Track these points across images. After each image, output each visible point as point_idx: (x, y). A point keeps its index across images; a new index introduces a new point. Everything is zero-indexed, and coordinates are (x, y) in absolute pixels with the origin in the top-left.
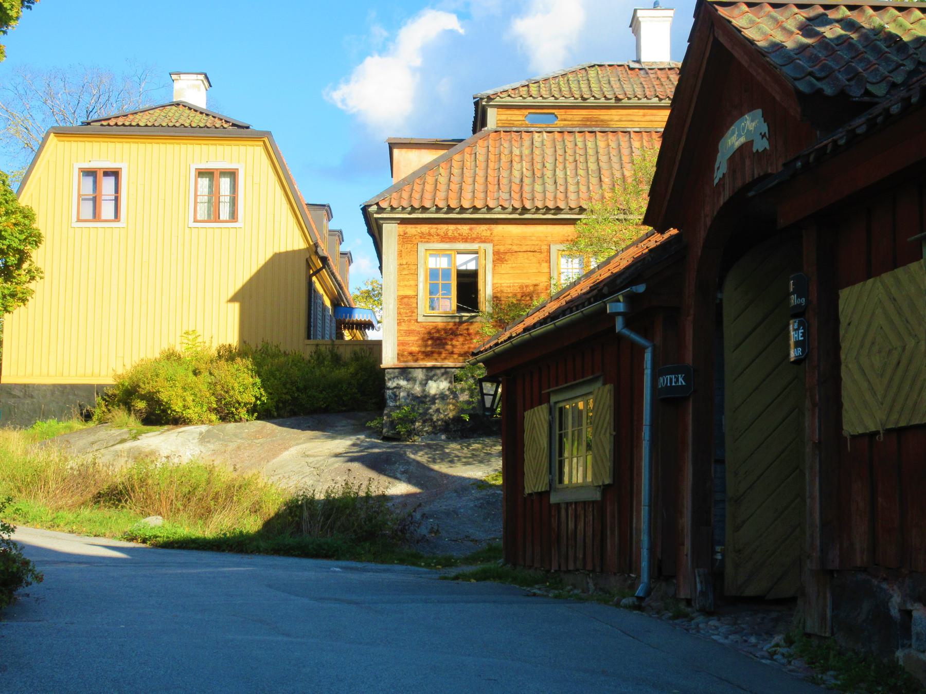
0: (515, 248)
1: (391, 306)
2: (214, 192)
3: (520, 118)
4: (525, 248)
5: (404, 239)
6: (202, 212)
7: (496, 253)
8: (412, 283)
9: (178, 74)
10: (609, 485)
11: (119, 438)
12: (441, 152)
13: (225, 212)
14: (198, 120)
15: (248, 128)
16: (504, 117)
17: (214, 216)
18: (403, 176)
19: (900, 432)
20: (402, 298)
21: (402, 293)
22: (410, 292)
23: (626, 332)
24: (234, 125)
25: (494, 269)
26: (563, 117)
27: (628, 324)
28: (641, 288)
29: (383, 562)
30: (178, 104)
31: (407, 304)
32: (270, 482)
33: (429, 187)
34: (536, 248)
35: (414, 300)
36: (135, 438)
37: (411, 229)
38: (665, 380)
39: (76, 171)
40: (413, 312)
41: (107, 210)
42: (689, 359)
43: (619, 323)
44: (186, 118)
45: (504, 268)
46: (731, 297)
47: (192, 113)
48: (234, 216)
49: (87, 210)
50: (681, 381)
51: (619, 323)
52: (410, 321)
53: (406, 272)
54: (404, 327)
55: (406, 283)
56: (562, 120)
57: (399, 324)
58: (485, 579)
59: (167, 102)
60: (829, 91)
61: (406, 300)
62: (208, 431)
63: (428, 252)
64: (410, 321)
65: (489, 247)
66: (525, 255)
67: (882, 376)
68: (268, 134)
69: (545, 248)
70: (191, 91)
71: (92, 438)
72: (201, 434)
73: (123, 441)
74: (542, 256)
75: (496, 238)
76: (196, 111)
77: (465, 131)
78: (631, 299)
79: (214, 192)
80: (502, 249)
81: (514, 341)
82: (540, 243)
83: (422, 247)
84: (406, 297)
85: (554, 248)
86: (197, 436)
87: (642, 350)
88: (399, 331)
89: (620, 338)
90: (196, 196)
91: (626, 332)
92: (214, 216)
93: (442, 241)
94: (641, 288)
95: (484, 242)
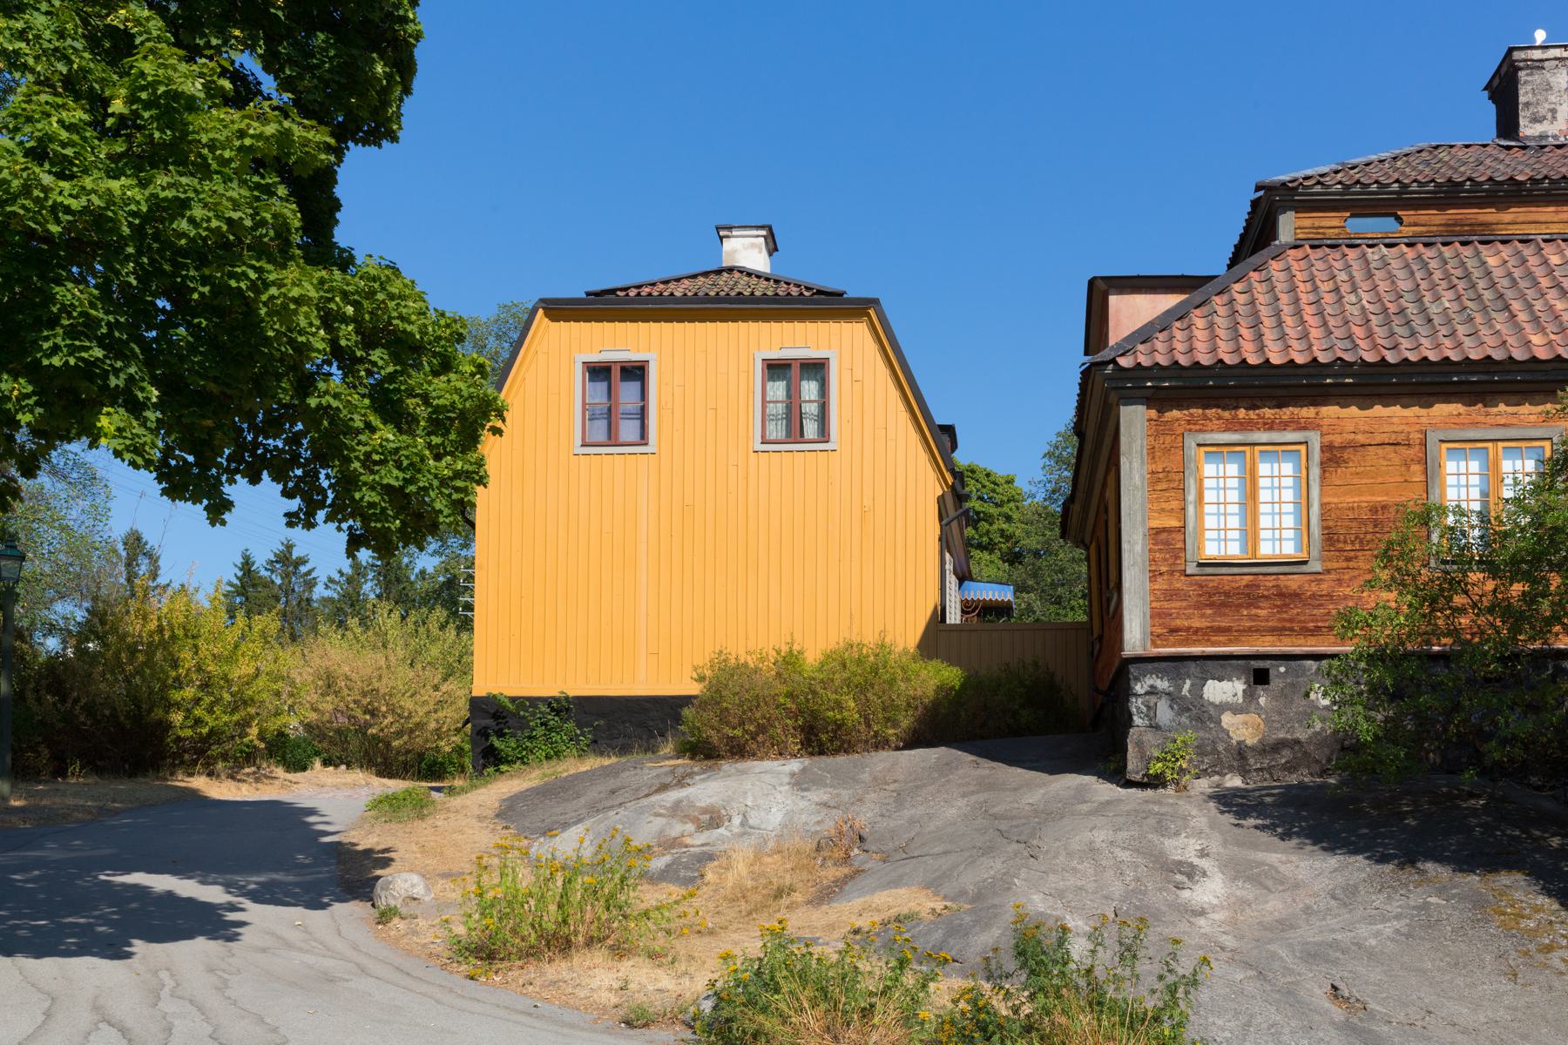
0: (1361, 438)
1: (1138, 548)
2: (793, 397)
3: (1335, 223)
4: (1379, 439)
5: (1159, 430)
6: (776, 430)
7: (1327, 448)
8: (1175, 504)
9: (730, 228)
11: (657, 783)
12: (1170, 301)
13: (811, 429)
14: (761, 288)
15: (841, 295)
16: (1307, 223)
17: (795, 432)
18: (1126, 333)
21: (1156, 524)
24: (819, 292)
25: (1323, 478)
26: (1412, 219)
29: (602, 754)
30: (730, 270)
31: (1167, 543)
32: (241, 620)
33: (1200, 335)
34: (1400, 438)
35: (1180, 537)
36: (681, 784)
39: (579, 369)
40: (1177, 558)
41: (628, 430)
44: (743, 285)
45: (1339, 475)
47: (754, 280)
48: (824, 434)
49: (599, 430)
52: (1171, 573)
53: (1164, 486)
54: (1161, 584)
55: (1164, 505)
56: (1410, 225)
57: (1153, 579)
59: (715, 268)
61: (1164, 536)
62: (804, 770)
63: (1203, 449)
64: (1171, 573)
65: (1315, 439)
66: (1380, 451)
68: (874, 302)
69: (1416, 437)
70: (747, 252)
71: (612, 783)
72: (792, 775)
73: (664, 788)
74: (1411, 452)
75: (1326, 422)
76: (758, 277)
77: (1216, 264)
79: (793, 397)
80: (1337, 440)
82: (1407, 429)
83: (1191, 442)
84: (1164, 530)
85: (1432, 438)
86: (787, 780)
88: (1152, 591)
90: (764, 402)
92: (795, 432)
93: (1227, 430)
95: (1305, 428)
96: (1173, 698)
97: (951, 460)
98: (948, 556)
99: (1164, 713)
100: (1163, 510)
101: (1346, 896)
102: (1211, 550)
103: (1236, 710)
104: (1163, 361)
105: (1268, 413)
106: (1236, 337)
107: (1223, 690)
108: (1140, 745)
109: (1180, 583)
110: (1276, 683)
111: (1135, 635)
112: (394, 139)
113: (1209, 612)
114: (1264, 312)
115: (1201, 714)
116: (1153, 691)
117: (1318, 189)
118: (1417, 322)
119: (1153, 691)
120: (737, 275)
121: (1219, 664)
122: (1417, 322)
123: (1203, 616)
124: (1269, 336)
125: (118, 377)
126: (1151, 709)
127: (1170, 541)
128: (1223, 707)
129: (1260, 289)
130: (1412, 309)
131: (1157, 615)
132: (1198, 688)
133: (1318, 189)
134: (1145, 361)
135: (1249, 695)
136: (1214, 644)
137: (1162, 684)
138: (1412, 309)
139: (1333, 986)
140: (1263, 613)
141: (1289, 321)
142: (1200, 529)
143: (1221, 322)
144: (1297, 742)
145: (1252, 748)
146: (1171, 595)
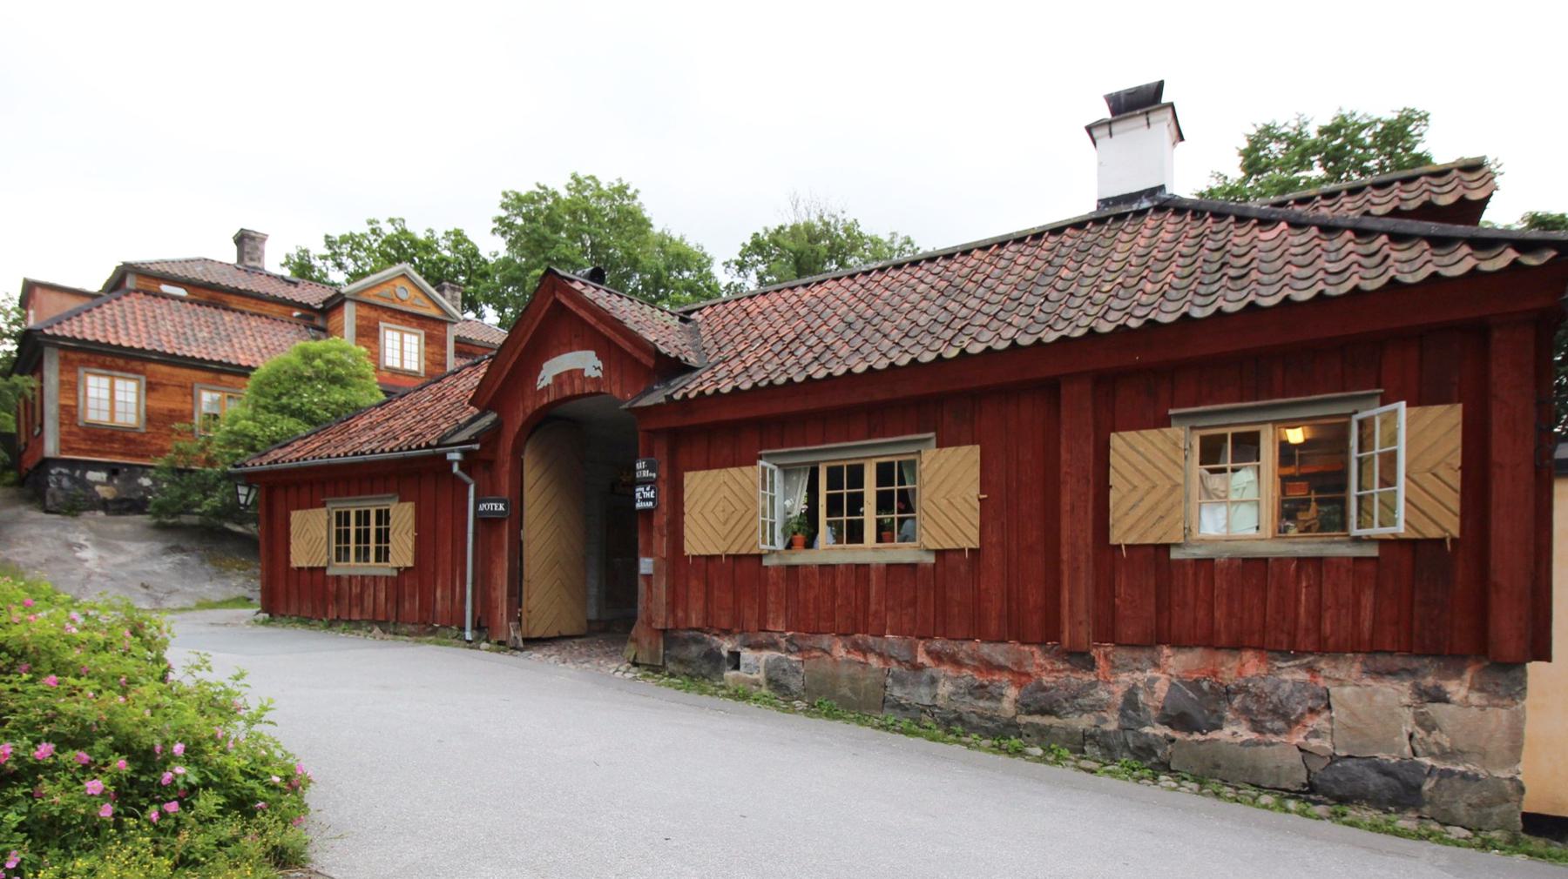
10: (407, 569)
19: (737, 558)
20: (63, 408)
22: (71, 403)
23: (462, 474)
27: (461, 468)
28: (477, 447)
37: (72, 356)
38: (483, 507)
42: (506, 496)
43: (456, 468)
46: (528, 460)
50: (501, 508)
51: (456, 468)
54: (65, 428)
58: (120, 512)
60: (1133, 323)
67: (725, 523)
78: (465, 453)
81: (280, 465)
87: (467, 486)
89: (455, 476)
91: (466, 478)
94: (477, 447)
96: (71, 477)
97: (421, 326)
98: (1550, 254)
99: (66, 483)
101: (152, 556)
103: (102, 484)
104: (68, 335)
106: (105, 331)
108: (53, 495)
109: (74, 429)
110: (122, 475)
111: (51, 448)
114: (120, 320)
116: (60, 473)
118: (191, 339)
119: (60, 473)
120: (977, 254)
121: (96, 466)
122: (191, 339)
124: (122, 333)
126: (59, 482)
127: (69, 413)
128: (96, 483)
129: (117, 310)
130: (189, 333)
131: (62, 441)
134: (58, 333)
135: (110, 479)
137: (65, 471)
138: (189, 333)
139: (143, 585)
141: (132, 327)
142: (86, 407)
143: (98, 321)
146: (70, 433)
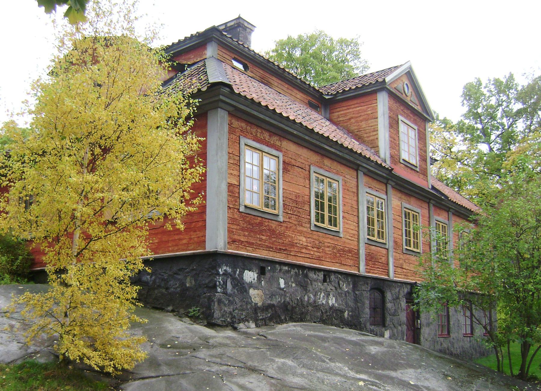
8: (235, 173)
100: (232, 174)
102: (248, 203)
105: (266, 135)
107: (250, 276)
110: (268, 275)
112: (239, 18)
113: (247, 233)
115: (242, 288)
116: (226, 274)
117: (230, 40)
123: (244, 236)
125: (453, 144)
132: (241, 273)
133: (230, 40)
135: (259, 279)
136: (248, 251)
140: (264, 238)
144: (273, 305)
145: (259, 308)
